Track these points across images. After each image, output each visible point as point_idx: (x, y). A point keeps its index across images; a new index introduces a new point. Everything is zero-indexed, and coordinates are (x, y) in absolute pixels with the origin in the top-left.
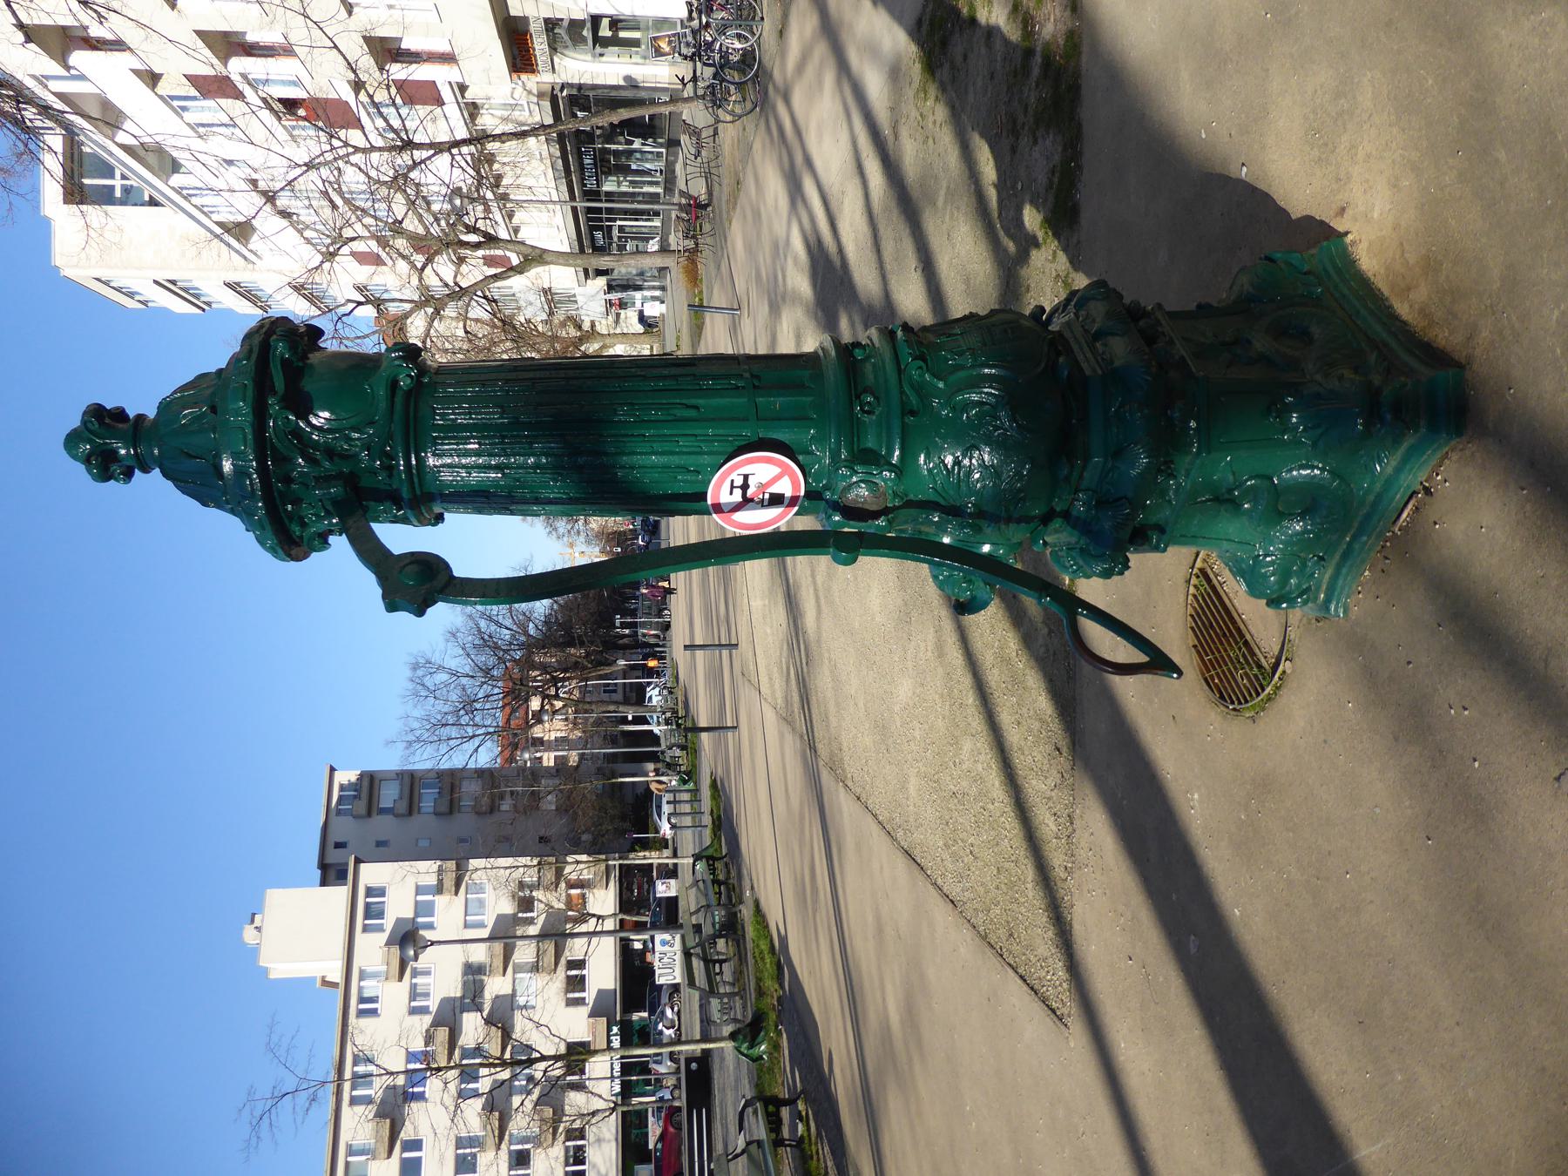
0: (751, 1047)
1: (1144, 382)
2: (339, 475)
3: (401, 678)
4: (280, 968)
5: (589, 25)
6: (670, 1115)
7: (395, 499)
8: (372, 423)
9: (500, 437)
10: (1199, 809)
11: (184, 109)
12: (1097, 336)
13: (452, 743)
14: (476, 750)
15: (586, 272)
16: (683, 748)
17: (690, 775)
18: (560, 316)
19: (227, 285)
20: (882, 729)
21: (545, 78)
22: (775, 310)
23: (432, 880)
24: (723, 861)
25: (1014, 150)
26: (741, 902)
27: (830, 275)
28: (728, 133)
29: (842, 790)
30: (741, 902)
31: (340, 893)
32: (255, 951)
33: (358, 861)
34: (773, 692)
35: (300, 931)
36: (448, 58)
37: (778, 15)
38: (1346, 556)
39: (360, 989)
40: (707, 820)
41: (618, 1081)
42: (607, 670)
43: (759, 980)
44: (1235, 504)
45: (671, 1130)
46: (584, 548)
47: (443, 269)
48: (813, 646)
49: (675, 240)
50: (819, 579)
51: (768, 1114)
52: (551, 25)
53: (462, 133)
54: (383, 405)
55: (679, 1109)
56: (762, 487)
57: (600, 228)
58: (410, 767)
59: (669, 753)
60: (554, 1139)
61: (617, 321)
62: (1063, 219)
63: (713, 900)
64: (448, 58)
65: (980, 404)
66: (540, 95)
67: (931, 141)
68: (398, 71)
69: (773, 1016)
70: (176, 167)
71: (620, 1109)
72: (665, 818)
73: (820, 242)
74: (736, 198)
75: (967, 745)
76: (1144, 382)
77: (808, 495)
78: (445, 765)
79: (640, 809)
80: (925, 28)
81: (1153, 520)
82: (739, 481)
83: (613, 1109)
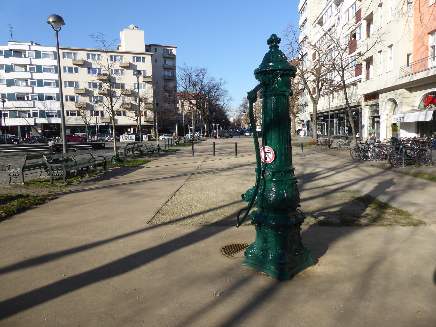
0: (115, 159)
1: (286, 230)
2: (270, 83)
3: (201, 67)
4: (123, 35)
5: (377, 115)
6: (84, 139)
7: (265, 92)
8: (279, 88)
9: (276, 110)
10: (201, 245)
11: (353, 8)
12: (296, 216)
13: (185, 80)
14: (183, 87)
15: (312, 115)
16: (185, 142)
17: (178, 144)
18: (300, 108)
19: (306, 19)
20: (202, 189)
21: (363, 104)
22: (302, 165)
23: (147, 75)
24: (158, 153)
25: (337, 215)
26: (149, 157)
27: (311, 177)
28: (348, 153)
29: (184, 181)
30: (149, 157)
31: (143, 50)
32: (127, 28)
33: (152, 55)
34: (203, 165)
35: (133, 40)
36: (368, 78)
37: (377, 165)
38: (255, 264)
39: (118, 56)
40: (167, 148)
41: (59, 121)
42: (203, 121)
43: (131, 161)
44: (265, 242)
45: (81, 139)
46: (236, 114)
47: (312, 78)
48: (218, 174)
49: (320, 139)
50: (235, 175)
51: (102, 163)
52: (377, 105)
53: (346, 82)
54: (282, 90)
55: (86, 141)
56: (268, 156)
57: (324, 119)
58: (177, 68)
59: (183, 138)
60: (79, 108)
61: (299, 123)
62: (321, 224)
63: (149, 150)
64: (368, 78)
65: (283, 194)
66: (359, 102)
67: (340, 199)
68: (364, 64)
69: (123, 165)
70: (337, 5)
71: (86, 125)
72: (164, 137)
73: (319, 175)
74: (331, 155)
75: (202, 206)
76: (286, 230)
77: (267, 164)
78: (178, 78)
79: (165, 130)
80: (368, 197)
81: (262, 228)
82: (269, 152)
83: (86, 124)
